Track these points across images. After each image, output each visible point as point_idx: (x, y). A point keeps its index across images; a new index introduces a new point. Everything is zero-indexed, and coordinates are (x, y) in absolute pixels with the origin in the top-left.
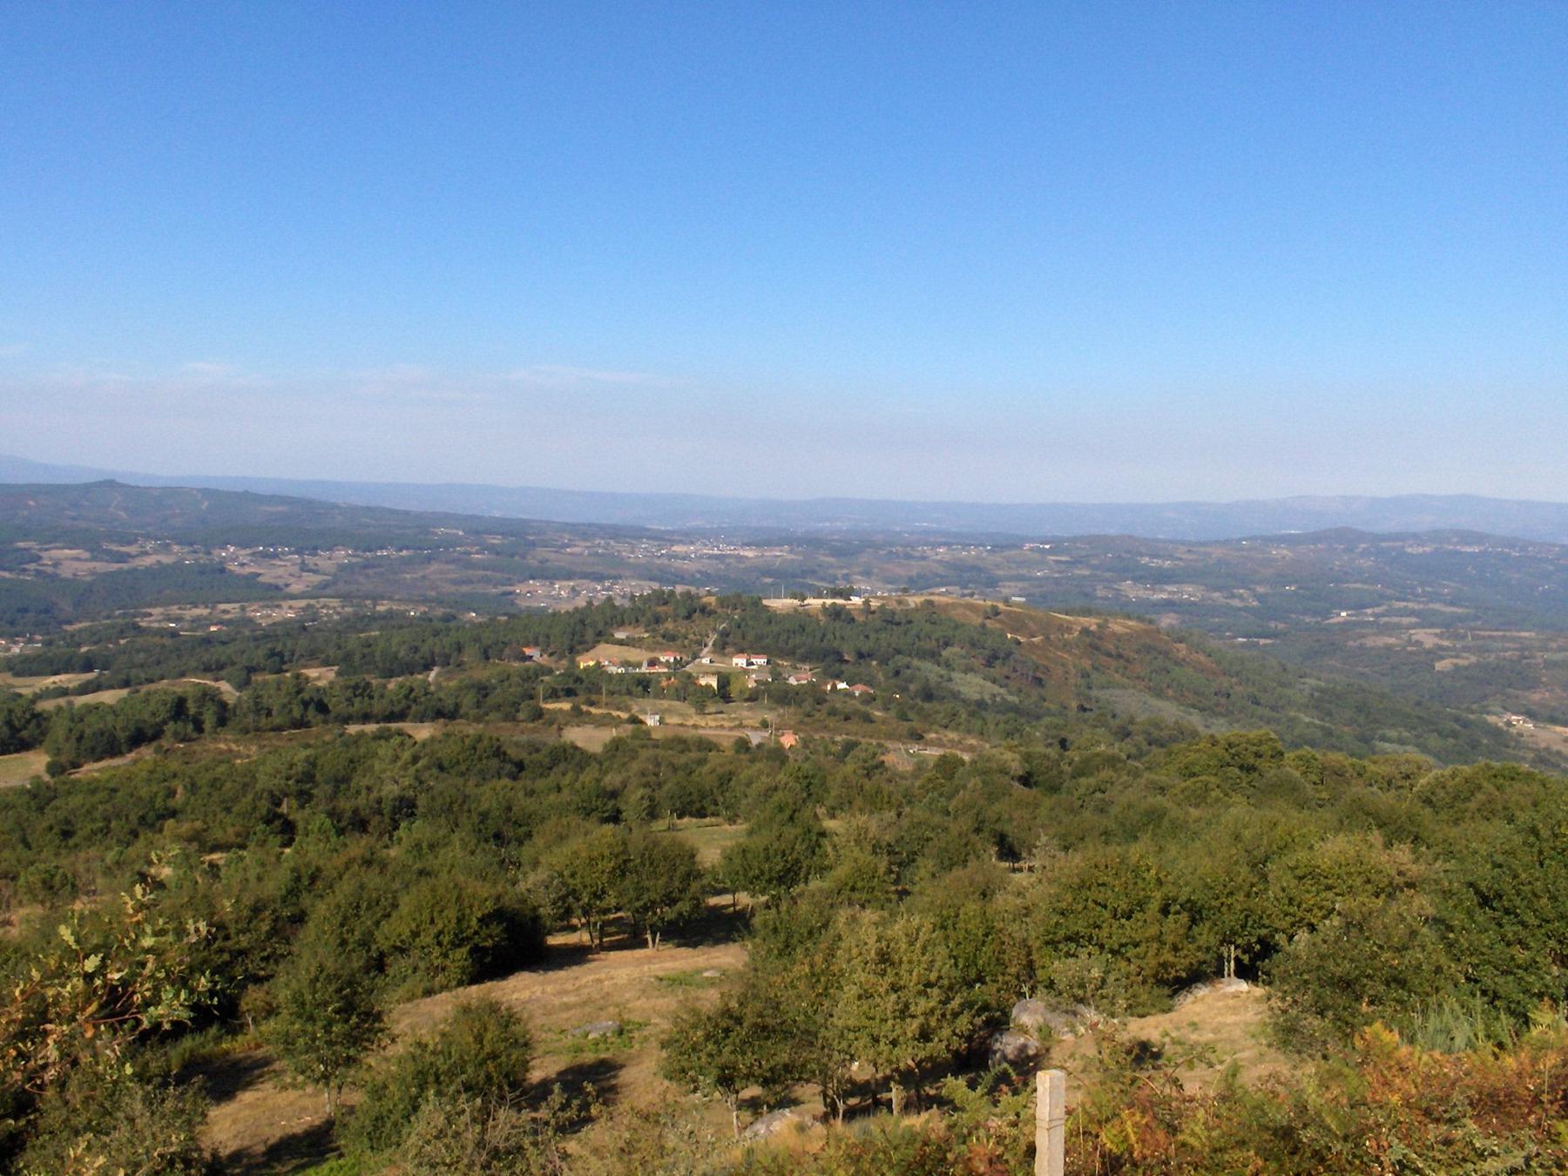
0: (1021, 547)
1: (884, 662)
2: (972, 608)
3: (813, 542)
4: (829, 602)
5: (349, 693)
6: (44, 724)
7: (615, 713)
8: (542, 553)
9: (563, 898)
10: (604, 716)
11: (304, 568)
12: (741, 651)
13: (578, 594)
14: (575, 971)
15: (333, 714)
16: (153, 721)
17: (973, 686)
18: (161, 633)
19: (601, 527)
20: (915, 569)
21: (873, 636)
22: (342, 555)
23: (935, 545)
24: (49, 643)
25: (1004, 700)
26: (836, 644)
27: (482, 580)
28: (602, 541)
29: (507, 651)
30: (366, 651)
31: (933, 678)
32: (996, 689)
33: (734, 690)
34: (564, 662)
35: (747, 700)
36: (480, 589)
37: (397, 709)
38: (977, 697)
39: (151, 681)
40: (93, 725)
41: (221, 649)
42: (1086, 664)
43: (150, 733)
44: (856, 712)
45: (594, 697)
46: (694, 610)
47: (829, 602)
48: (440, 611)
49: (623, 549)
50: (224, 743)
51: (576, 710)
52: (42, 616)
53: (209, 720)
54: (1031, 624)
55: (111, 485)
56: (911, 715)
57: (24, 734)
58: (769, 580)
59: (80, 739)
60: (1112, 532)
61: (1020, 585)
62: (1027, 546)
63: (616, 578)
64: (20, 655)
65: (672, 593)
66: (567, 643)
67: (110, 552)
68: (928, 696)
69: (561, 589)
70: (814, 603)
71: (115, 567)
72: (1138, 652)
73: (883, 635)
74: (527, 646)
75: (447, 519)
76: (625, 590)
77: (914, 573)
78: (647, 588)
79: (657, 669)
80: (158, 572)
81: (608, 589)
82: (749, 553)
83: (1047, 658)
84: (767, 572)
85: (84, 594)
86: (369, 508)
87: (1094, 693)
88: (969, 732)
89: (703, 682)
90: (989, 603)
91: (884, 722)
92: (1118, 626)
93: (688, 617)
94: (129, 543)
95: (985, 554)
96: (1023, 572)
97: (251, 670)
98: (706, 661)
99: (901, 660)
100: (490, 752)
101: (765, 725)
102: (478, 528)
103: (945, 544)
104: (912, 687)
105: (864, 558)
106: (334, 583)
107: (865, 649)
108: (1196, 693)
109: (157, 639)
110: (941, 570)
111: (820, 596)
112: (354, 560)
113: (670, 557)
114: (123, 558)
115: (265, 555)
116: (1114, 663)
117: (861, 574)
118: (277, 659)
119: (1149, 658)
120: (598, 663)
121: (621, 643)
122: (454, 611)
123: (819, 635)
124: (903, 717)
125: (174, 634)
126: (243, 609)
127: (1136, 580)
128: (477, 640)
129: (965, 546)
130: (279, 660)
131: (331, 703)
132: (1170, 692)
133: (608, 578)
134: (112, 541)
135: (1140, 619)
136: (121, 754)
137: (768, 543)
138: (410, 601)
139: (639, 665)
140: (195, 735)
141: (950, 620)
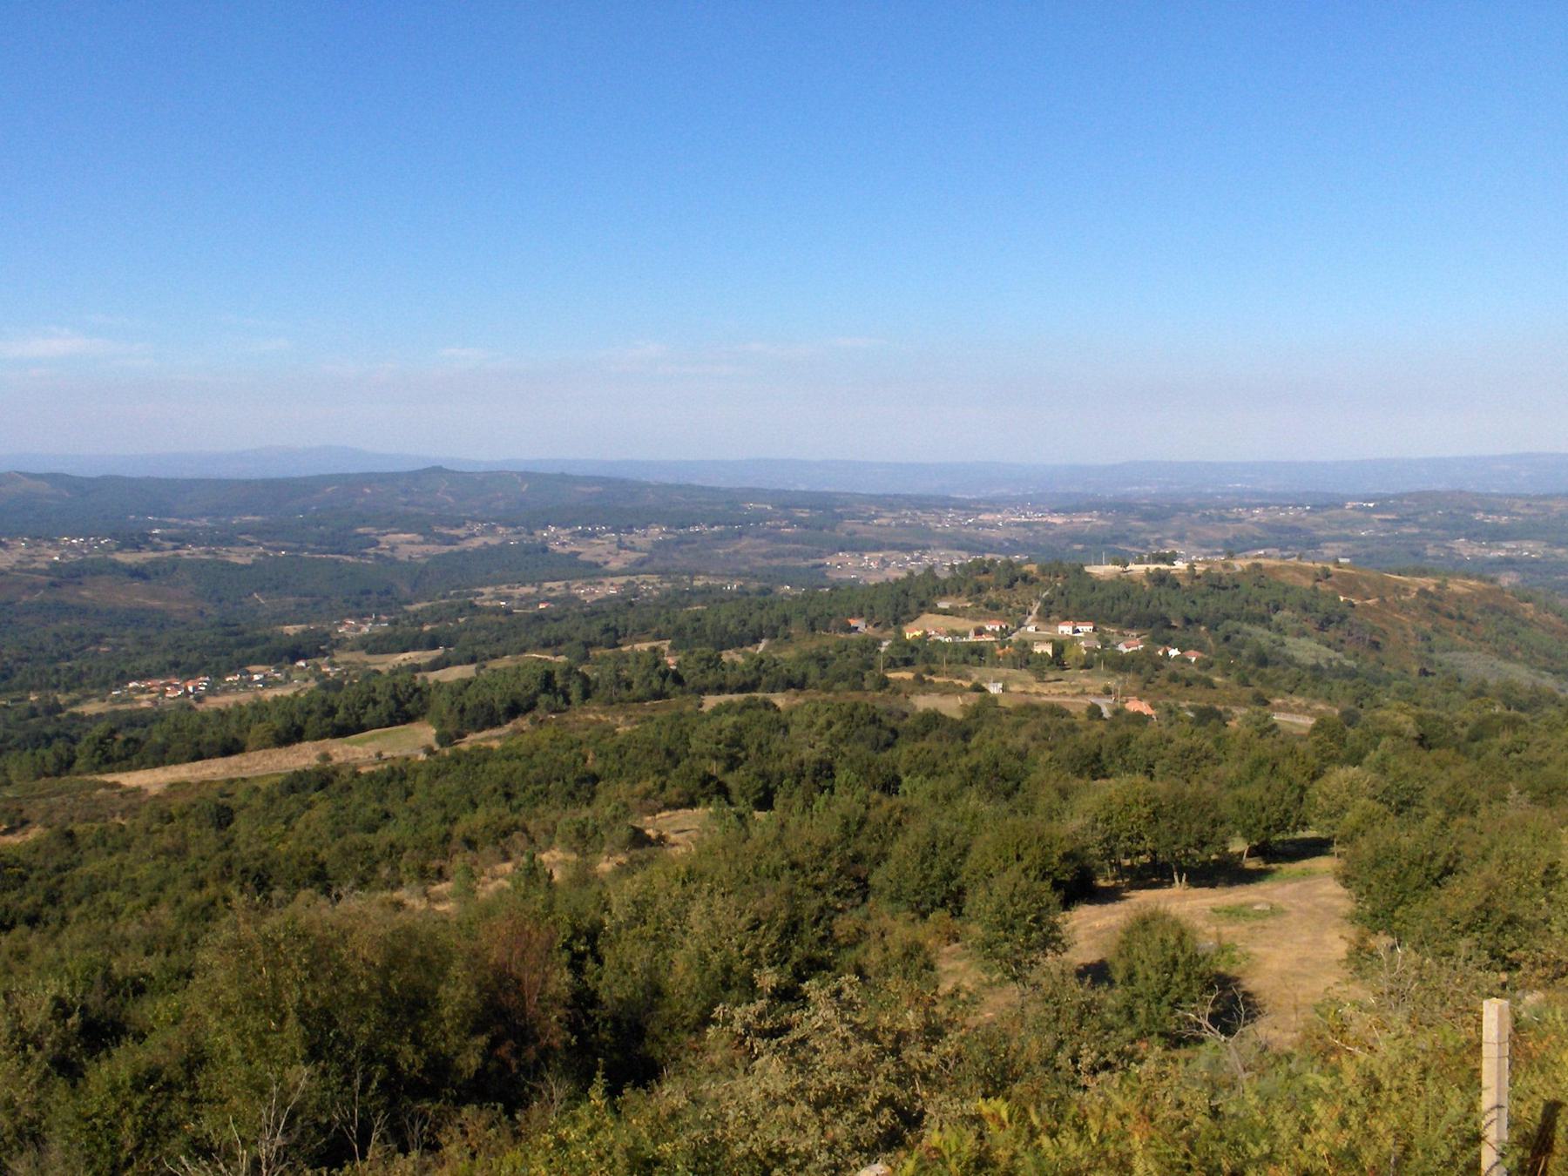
0: (1342, 506)
1: (1213, 627)
2: (1303, 571)
3: (1124, 507)
4: (1152, 567)
5: (702, 665)
6: (425, 697)
7: (958, 682)
8: (849, 525)
9: (1107, 840)
10: (947, 685)
11: (621, 545)
12: (1066, 619)
13: (888, 565)
14: (1253, 887)
15: (690, 685)
16: (525, 693)
17: (1306, 650)
18: (496, 611)
19: (908, 498)
20: (1231, 530)
21: (1200, 601)
22: (656, 532)
23: (1250, 507)
24: (394, 623)
25: (1341, 665)
26: (1163, 609)
27: (792, 553)
28: (908, 513)
29: (833, 623)
30: (696, 625)
31: (1265, 643)
32: (1331, 654)
33: (1069, 655)
34: (891, 632)
35: (1082, 668)
36: (790, 562)
37: (749, 679)
38: (1311, 662)
39: (494, 657)
40: (470, 699)
41: (555, 626)
42: (1426, 626)
43: (525, 704)
44: (1197, 678)
45: (933, 666)
46: (1015, 578)
47: (1152, 567)
48: (754, 586)
49: (930, 520)
50: (593, 713)
51: (919, 678)
52: (383, 598)
53: (575, 692)
54: (1365, 586)
55: (437, 471)
56: (1252, 680)
57: (408, 706)
58: (1079, 547)
59: (462, 711)
60: (1441, 486)
61: (1344, 545)
62: (1349, 505)
63: (925, 548)
64: (370, 635)
65: (993, 562)
66: (891, 613)
67: (441, 536)
68: (1263, 661)
69: (871, 560)
70: (1137, 569)
71: (446, 549)
72: (1482, 612)
73: (1211, 600)
74: (852, 616)
75: (753, 494)
76: (945, 561)
77: (1229, 536)
78: (960, 558)
79: (985, 638)
80: (486, 553)
81: (918, 559)
82: (1058, 520)
83: (1384, 621)
84: (1075, 538)
85: (419, 576)
86: (680, 487)
87: (1437, 656)
88: (1315, 697)
89: (1038, 649)
90: (1319, 565)
91: (1226, 687)
92: (1457, 587)
93: (1010, 586)
94: (458, 526)
95: (1306, 515)
96: (1347, 532)
97: (588, 645)
98: (1031, 629)
99: (1231, 625)
100: (867, 719)
101: (1108, 692)
102: (787, 502)
103: (1261, 505)
104: (1245, 653)
105: (1175, 522)
106: (650, 560)
107: (1192, 616)
108: (1549, 656)
109: (492, 617)
110: (1257, 532)
111: (1141, 562)
112: (669, 537)
113: (977, 526)
114: (452, 540)
115: (583, 534)
116: (1457, 625)
117: (1174, 538)
118: (612, 634)
119: (1493, 618)
120: (925, 633)
121: (945, 612)
122: (768, 585)
123: (1144, 601)
124: (1245, 683)
125: (508, 612)
126: (567, 587)
127: (1469, 537)
128: (804, 612)
129: (1283, 506)
130: (614, 636)
131: (686, 675)
132: (1519, 654)
133: (917, 548)
134: (442, 525)
135: (1480, 578)
136: (499, 724)
137: (1079, 509)
138: (723, 575)
139: (966, 634)
140: (565, 707)
141: (1279, 582)
